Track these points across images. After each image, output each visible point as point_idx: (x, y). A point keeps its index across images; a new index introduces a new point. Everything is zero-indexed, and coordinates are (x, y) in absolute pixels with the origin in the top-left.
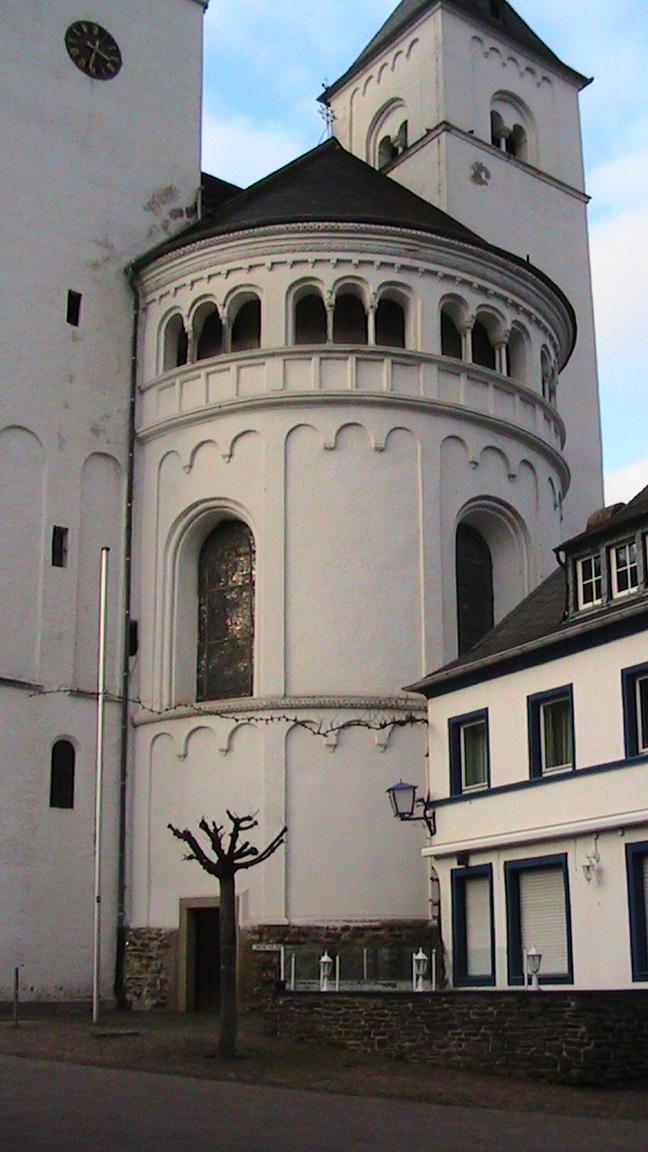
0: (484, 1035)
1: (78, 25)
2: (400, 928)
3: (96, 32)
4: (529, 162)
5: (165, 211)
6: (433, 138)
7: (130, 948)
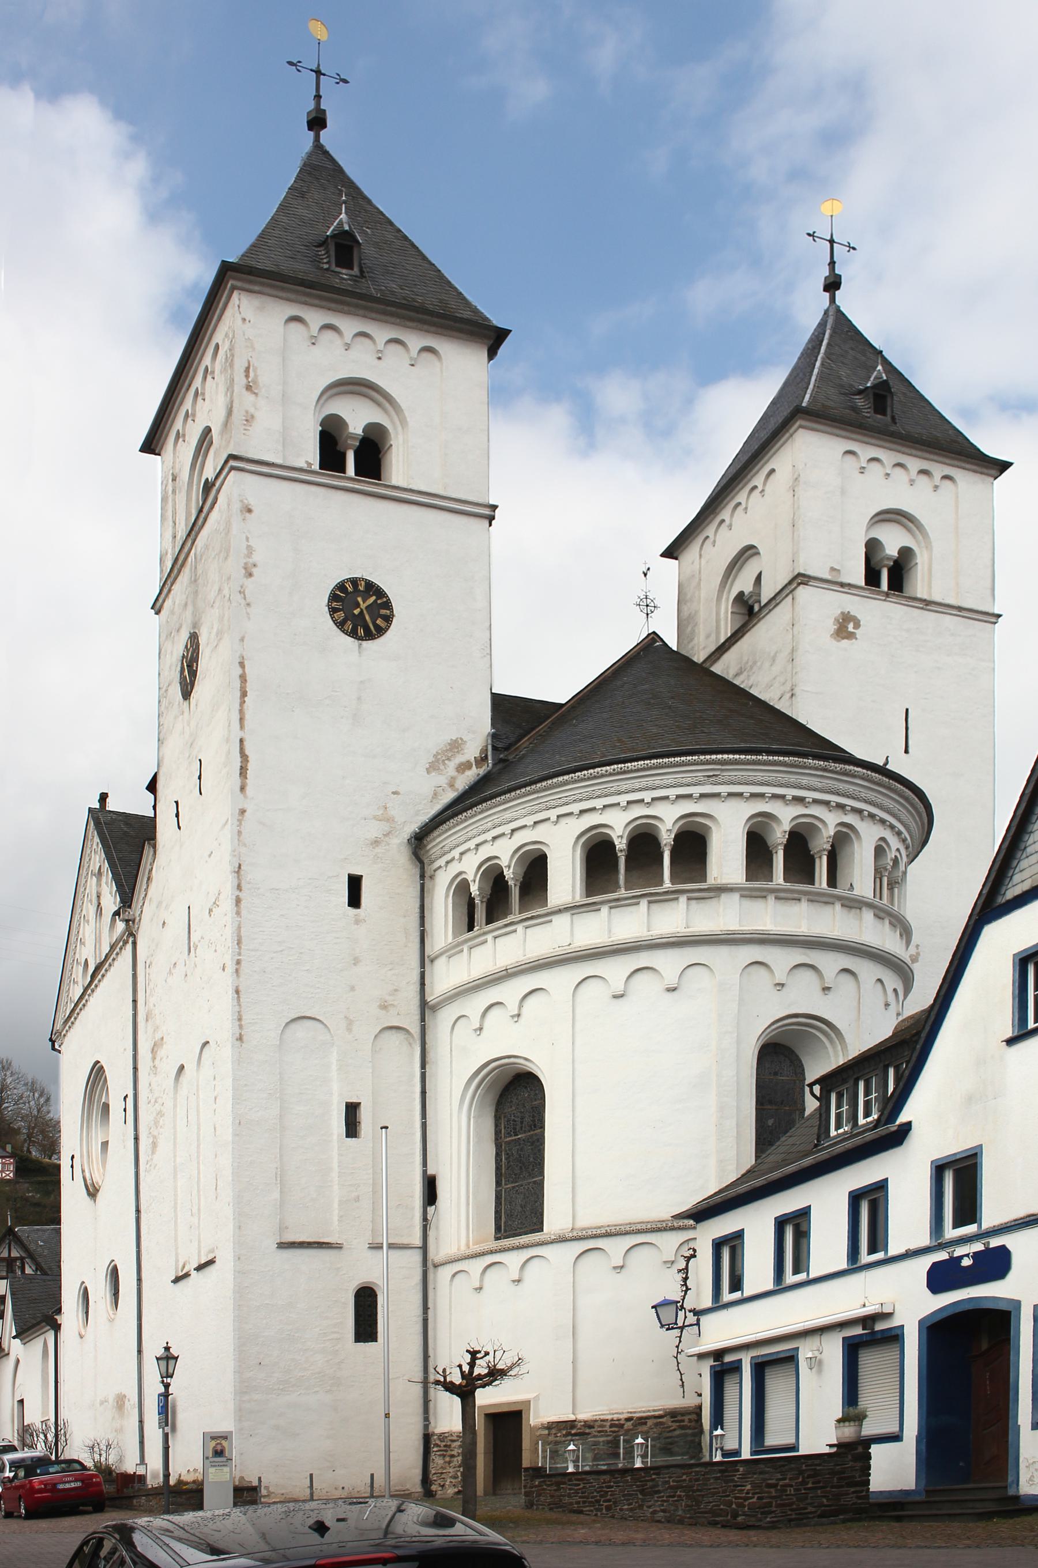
0: (679, 1496)
1: (341, 586)
2: (683, 1414)
3: (349, 625)
4: (919, 596)
5: (452, 765)
6: (787, 596)
7: (435, 1449)
